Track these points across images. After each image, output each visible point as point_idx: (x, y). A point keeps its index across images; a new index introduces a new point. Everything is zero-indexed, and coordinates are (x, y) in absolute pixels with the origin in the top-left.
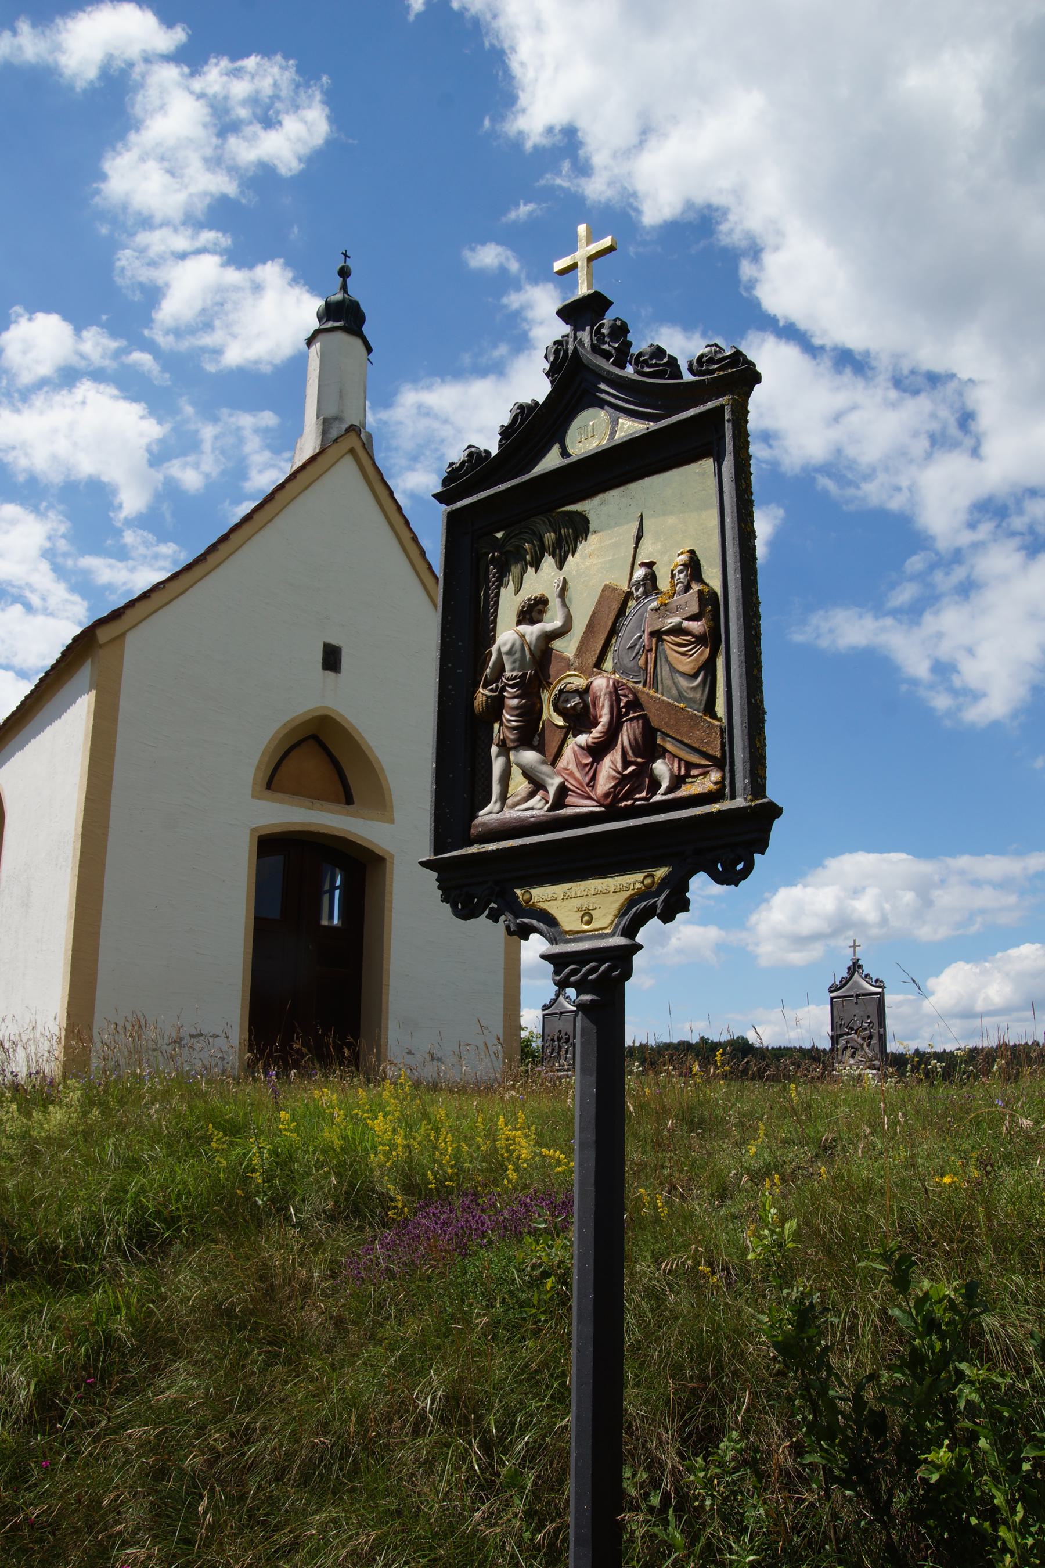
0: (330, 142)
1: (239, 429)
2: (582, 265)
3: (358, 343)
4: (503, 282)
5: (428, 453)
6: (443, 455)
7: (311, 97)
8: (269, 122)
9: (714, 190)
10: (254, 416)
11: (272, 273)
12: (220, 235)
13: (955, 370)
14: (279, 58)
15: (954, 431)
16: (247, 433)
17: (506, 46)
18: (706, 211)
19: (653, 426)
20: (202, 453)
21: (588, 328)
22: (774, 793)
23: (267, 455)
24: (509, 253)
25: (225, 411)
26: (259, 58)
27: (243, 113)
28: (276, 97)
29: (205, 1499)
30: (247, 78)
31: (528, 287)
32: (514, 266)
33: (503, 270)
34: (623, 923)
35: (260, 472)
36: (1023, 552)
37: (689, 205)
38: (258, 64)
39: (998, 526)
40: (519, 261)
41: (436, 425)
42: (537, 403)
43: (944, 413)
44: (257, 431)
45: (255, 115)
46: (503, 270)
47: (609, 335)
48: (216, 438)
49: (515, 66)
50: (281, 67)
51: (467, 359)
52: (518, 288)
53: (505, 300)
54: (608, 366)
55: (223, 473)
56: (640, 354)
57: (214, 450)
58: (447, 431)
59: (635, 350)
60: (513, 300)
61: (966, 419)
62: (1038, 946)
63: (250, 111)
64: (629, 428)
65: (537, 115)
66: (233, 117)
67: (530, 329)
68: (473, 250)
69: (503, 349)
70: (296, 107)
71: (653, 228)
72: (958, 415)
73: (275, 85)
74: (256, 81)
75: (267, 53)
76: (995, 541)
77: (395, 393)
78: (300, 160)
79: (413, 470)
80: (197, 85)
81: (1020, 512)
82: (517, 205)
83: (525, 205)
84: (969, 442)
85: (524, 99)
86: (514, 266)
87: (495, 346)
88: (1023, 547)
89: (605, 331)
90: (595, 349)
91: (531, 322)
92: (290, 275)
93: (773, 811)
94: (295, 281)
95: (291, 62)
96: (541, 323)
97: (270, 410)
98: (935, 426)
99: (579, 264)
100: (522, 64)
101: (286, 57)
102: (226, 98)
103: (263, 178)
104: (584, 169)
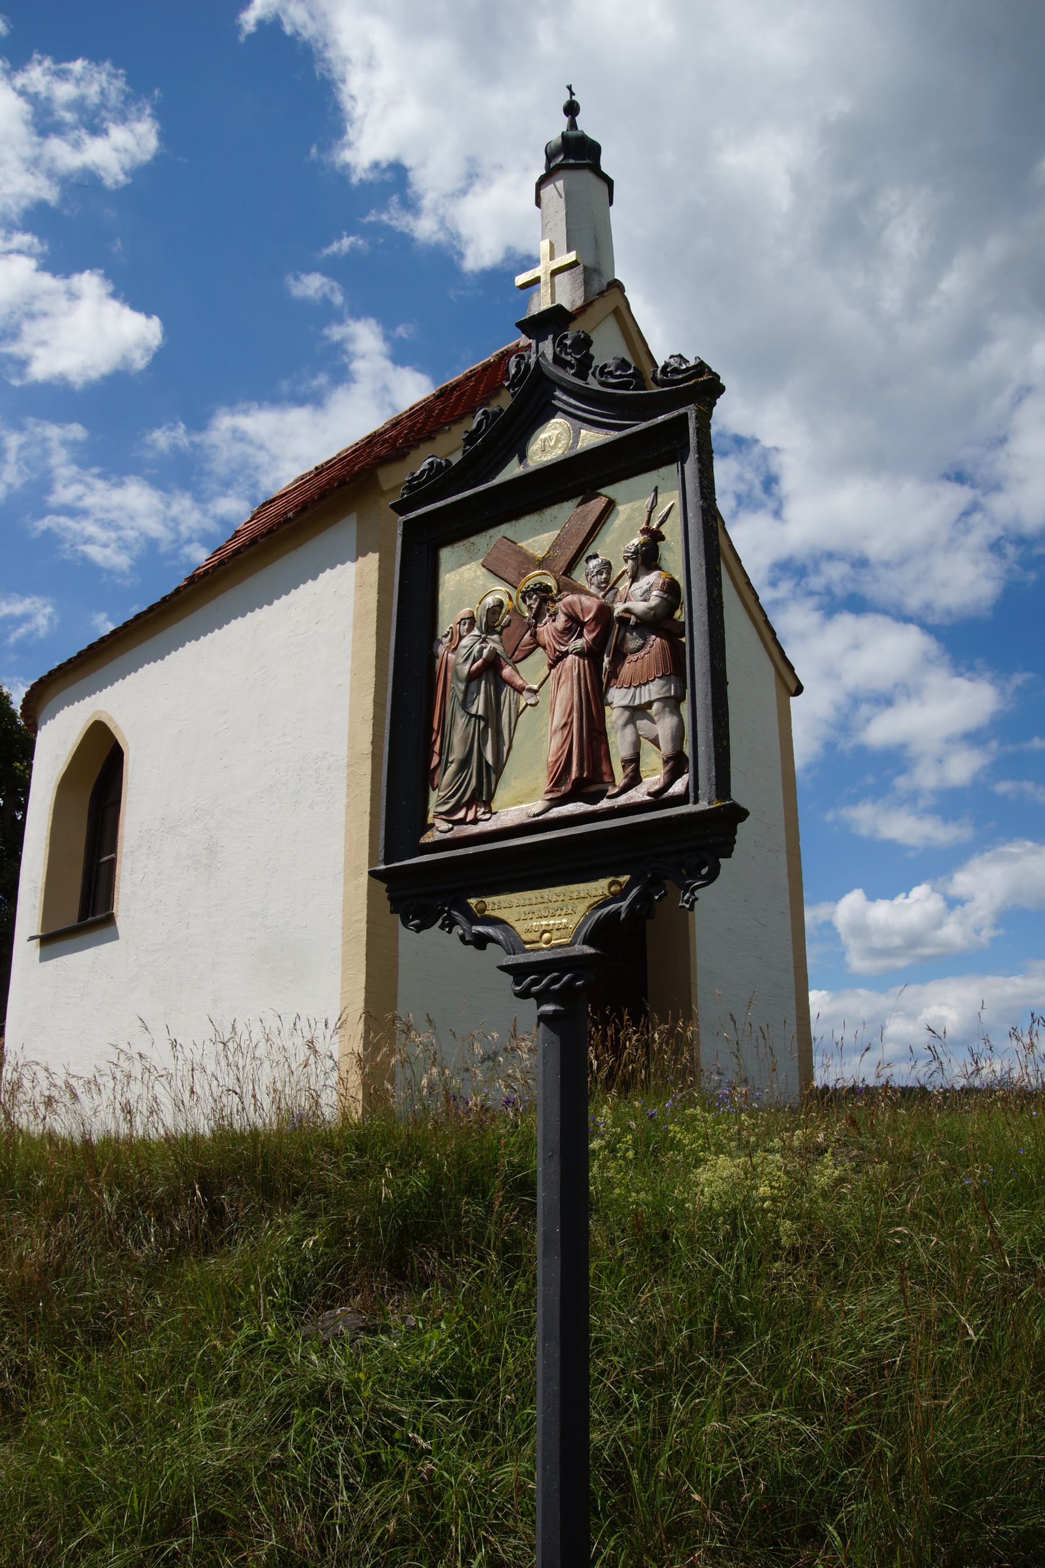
0: (158, 158)
1: (45, 440)
2: (545, 279)
4: (325, 313)
5: (241, 479)
6: (258, 482)
7: (140, 110)
8: (97, 130)
10: (62, 428)
11: (89, 283)
12: (36, 240)
13: (759, 437)
14: (108, 65)
15: (758, 492)
16: (54, 445)
17: (336, 76)
19: (614, 435)
20: (6, 462)
21: (550, 337)
22: (739, 795)
23: (74, 468)
24: (335, 284)
25: (31, 421)
26: (86, 62)
27: (69, 117)
28: (103, 106)
29: (899, 1229)
30: (72, 81)
31: (350, 322)
32: (338, 299)
33: (326, 301)
34: (597, 916)
35: (65, 486)
36: (822, 612)
38: (84, 68)
39: (798, 585)
40: (344, 294)
41: (251, 450)
42: (501, 410)
43: (749, 475)
44: (64, 443)
45: (81, 120)
46: (326, 301)
47: (571, 346)
48: (21, 448)
49: (344, 98)
50: (109, 74)
51: (285, 386)
52: (341, 321)
53: (326, 331)
54: (568, 375)
55: (26, 485)
56: (605, 366)
57: (17, 462)
58: (262, 458)
59: (597, 362)
60: (336, 333)
61: (770, 482)
62: (824, 992)
63: (76, 116)
64: (591, 438)
65: (366, 147)
66: (56, 117)
67: (350, 363)
68: (297, 278)
69: (322, 379)
70: (123, 118)
71: (473, 272)
72: (762, 478)
73: (102, 92)
74: (83, 84)
75: (95, 57)
76: (795, 599)
78: (126, 173)
79: (225, 496)
80: (20, 80)
81: (817, 571)
82: (340, 238)
83: (348, 237)
84: (772, 505)
85: (351, 134)
86: (338, 299)
87: (315, 376)
88: (820, 607)
89: (568, 342)
90: (557, 360)
91: (352, 356)
92: (111, 288)
93: (739, 814)
94: (114, 295)
95: (121, 71)
96: (363, 357)
97: (79, 423)
98: (742, 488)
99: (542, 279)
100: (352, 97)
101: (116, 66)
102: (49, 99)
103: (84, 185)
104: (411, 205)
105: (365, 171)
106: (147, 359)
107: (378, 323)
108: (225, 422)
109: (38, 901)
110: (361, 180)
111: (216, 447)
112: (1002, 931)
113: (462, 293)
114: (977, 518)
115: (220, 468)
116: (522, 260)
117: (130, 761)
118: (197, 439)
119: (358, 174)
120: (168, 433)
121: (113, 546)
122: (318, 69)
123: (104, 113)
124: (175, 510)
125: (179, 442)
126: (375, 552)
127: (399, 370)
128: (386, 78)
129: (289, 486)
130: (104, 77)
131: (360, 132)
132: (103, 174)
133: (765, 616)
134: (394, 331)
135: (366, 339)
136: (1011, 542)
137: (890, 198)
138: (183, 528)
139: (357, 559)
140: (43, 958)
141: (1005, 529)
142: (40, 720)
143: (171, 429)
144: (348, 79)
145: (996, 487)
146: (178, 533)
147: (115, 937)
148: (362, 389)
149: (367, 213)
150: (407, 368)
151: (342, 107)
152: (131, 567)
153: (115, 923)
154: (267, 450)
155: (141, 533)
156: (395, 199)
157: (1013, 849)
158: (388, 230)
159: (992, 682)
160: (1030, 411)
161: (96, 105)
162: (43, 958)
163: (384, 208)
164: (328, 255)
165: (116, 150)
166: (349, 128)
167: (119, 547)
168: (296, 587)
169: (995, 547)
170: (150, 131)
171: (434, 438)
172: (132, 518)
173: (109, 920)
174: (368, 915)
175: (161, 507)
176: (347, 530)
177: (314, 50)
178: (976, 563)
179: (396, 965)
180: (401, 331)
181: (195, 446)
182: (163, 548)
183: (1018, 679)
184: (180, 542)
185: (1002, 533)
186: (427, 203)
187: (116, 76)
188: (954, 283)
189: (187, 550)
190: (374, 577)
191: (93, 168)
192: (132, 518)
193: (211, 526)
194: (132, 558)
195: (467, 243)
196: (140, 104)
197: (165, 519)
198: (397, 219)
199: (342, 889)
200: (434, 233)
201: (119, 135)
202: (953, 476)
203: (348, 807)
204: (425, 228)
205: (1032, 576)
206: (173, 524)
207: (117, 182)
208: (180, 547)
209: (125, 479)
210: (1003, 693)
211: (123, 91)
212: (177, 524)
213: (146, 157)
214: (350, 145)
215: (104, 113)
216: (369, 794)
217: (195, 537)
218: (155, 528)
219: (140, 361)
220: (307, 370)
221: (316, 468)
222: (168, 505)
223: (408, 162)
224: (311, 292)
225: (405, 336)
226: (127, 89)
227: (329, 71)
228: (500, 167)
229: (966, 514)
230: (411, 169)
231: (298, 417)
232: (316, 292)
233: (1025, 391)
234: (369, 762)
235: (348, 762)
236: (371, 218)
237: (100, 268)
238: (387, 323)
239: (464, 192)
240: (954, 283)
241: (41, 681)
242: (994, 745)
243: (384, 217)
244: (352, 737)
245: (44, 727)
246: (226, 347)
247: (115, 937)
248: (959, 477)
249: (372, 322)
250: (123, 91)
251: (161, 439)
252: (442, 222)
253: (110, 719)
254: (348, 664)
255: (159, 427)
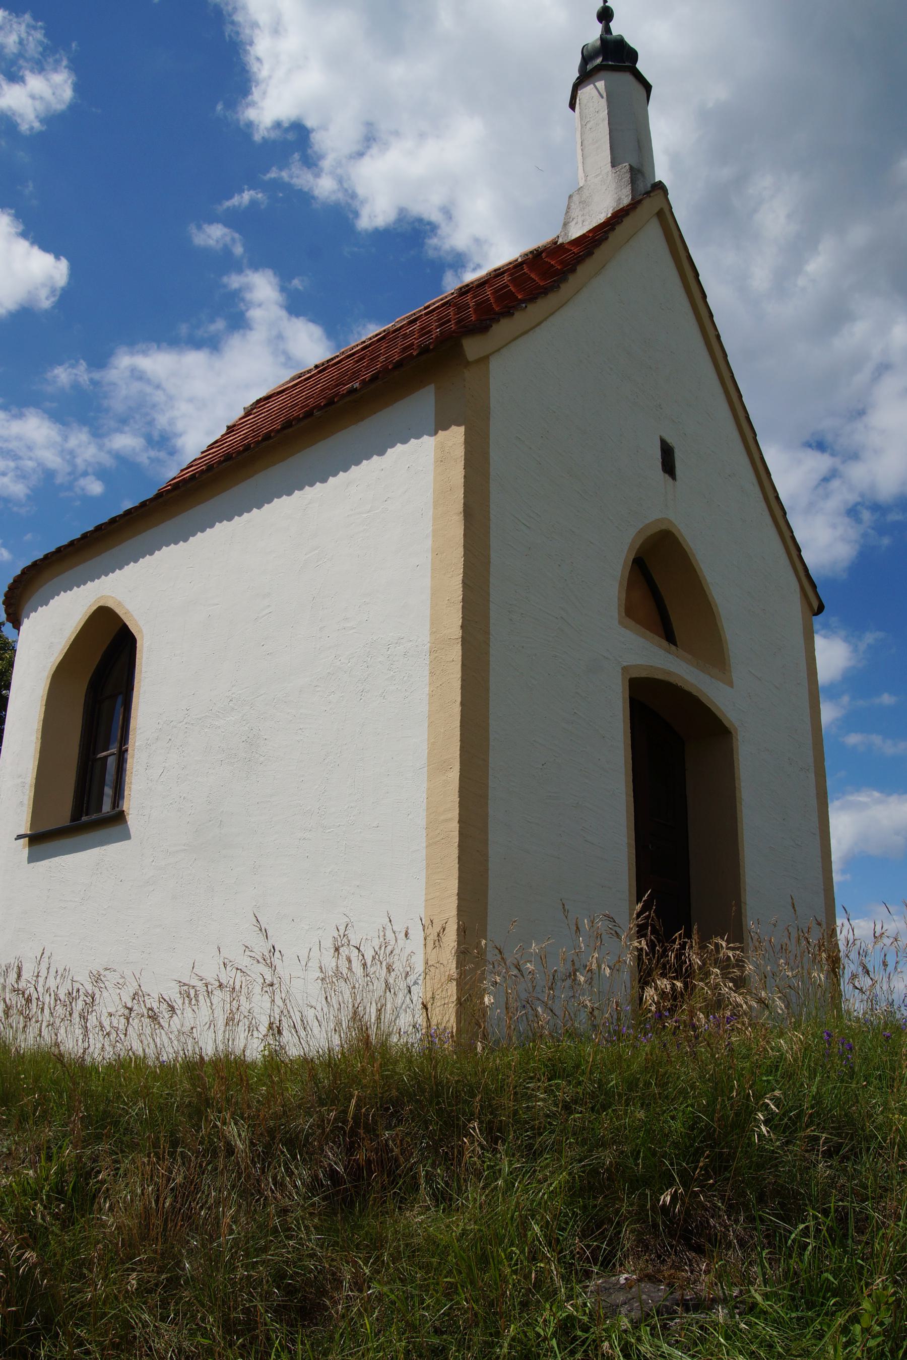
0: (73, 107)
3: (628, 77)
4: (226, 262)
5: (138, 417)
6: (154, 420)
7: (57, 62)
9: (427, 207)
14: (27, 17)
18: (416, 224)
26: (7, 13)
28: (20, 55)
31: (249, 272)
32: (238, 250)
33: (227, 252)
37: (402, 213)
38: (4, 17)
46: (227, 252)
49: (251, 60)
51: (184, 329)
52: (240, 271)
53: (225, 279)
60: (234, 281)
65: (272, 105)
67: (247, 310)
68: (199, 228)
69: (220, 325)
70: (40, 68)
71: (366, 231)
73: (21, 42)
77: (110, 354)
78: (42, 121)
79: (122, 432)
82: (241, 191)
85: (256, 94)
86: (238, 250)
87: (212, 320)
91: (250, 305)
94: (24, 235)
95: (40, 24)
96: (260, 305)
100: (258, 59)
101: (36, 18)
104: (311, 162)
105: (267, 129)
106: (53, 299)
107: (275, 274)
108: (125, 361)
109: (27, 797)
110: (263, 138)
111: (115, 384)
112: (848, 877)
113: (356, 249)
114: (835, 484)
115: (118, 405)
116: (413, 222)
117: (145, 649)
118: (96, 376)
119: (261, 132)
120: (70, 370)
121: (11, 474)
122: (228, 29)
123: (21, 62)
124: (72, 443)
125: (81, 379)
126: (459, 425)
127: (294, 320)
128: (292, 43)
129: (283, 385)
130: (23, 28)
131: (264, 93)
132: (19, 121)
133: (792, 532)
134: (290, 283)
135: (262, 289)
136: (867, 508)
137: (764, 182)
138: (79, 461)
139: (436, 433)
140: (32, 859)
141: (862, 495)
142: (24, 613)
143: (72, 366)
144: (255, 41)
145: (854, 456)
146: (74, 466)
147: (126, 836)
148: (258, 336)
149: (267, 170)
150: (301, 318)
151: (247, 68)
152: (28, 497)
153: (126, 822)
154: (164, 390)
155: (39, 464)
156: (296, 156)
157: (862, 798)
158: (287, 187)
159: (846, 640)
160: (889, 385)
161: (13, 54)
162: (32, 859)
163: (284, 164)
164: (228, 208)
165: (33, 97)
166: (254, 89)
167: (17, 476)
168: (357, 463)
169: (853, 512)
170: (66, 82)
171: (513, 314)
172: (30, 448)
173: (118, 818)
174: (460, 814)
175: (58, 439)
176: (424, 401)
177: (224, 13)
178: (834, 526)
179: (486, 870)
180: (296, 283)
181: (95, 383)
182: (59, 480)
183: (870, 638)
184: (75, 474)
185: (859, 499)
186: (327, 164)
187: (35, 28)
188: (819, 265)
189: (82, 482)
190: (459, 452)
191: (9, 113)
192: (30, 448)
193: (107, 461)
194: (29, 488)
195: (362, 202)
196: (58, 56)
197: (62, 451)
198: (298, 177)
199: (425, 785)
200: (334, 192)
201: (35, 83)
202: (814, 444)
203: (431, 696)
204: (325, 187)
205: (886, 541)
206: (70, 456)
207: (32, 128)
208: (76, 479)
209: (24, 410)
210: (855, 650)
211: (41, 43)
212: (74, 457)
213: (60, 107)
214: (253, 104)
215: (21, 62)
216: (459, 683)
217: (90, 470)
218: (52, 459)
219: (45, 303)
220: (201, 314)
221: (316, 367)
222: (66, 438)
223: (310, 123)
224: (212, 242)
225: (301, 288)
226: (46, 41)
227: (238, 33)
228: (397, 134)
229: (826, 480)
230: (313, 130)
231: (194, 359)
232: (217, 241)
233: (884, 368)
234: (459, 647)
235: (431, 648)
236: (273, 174)
237: (11, 208)
238: (284, 275)
239: (361, 154)
240: (819, 265)
241: (35, 564)
242: (846, 699)
243: (284, 175)
244: (435, 621)
245: (33, 615)
246: (139, 286)
247: (126, 836)
248: (820, 445)
249: (269, 273)
250: (41, 43)
251: (62, 375)
252: (340, 181)
253: (119, 604)
254: (429, 543)
255: (61, 364)
